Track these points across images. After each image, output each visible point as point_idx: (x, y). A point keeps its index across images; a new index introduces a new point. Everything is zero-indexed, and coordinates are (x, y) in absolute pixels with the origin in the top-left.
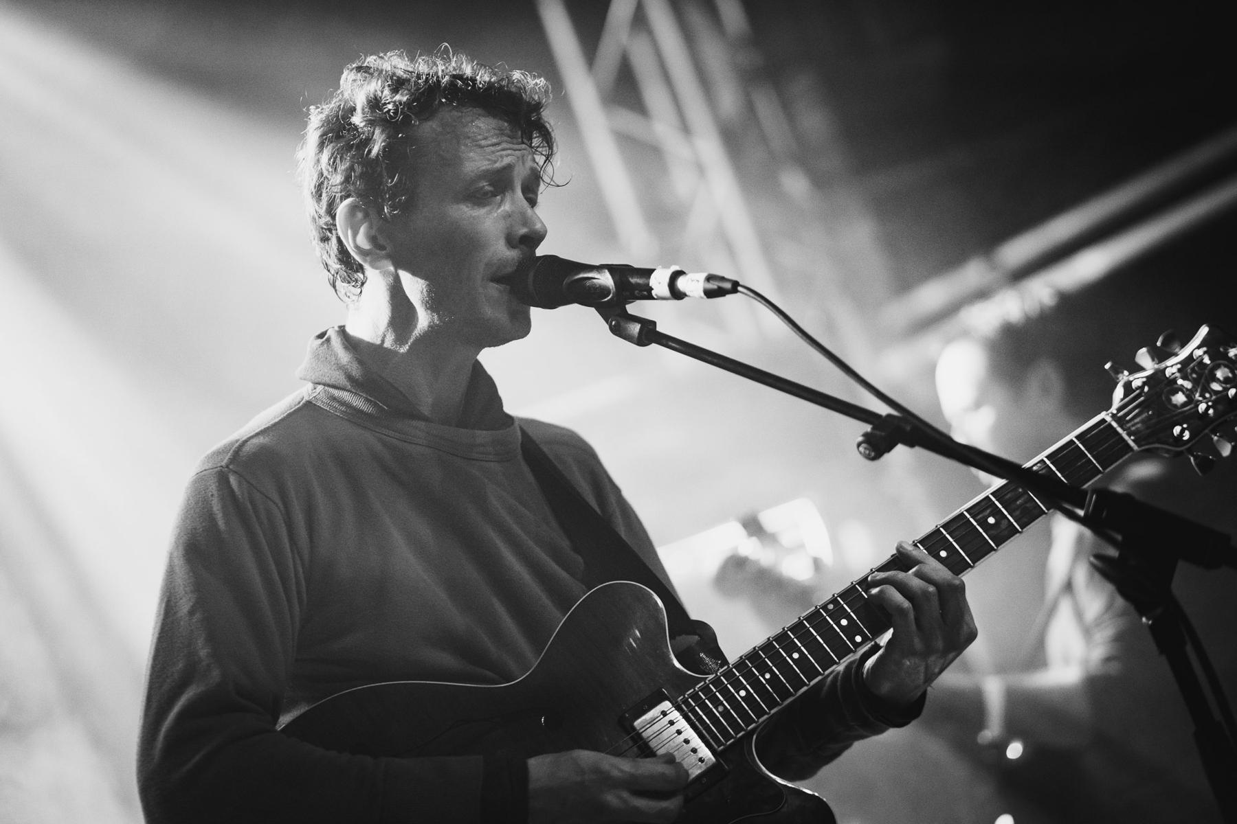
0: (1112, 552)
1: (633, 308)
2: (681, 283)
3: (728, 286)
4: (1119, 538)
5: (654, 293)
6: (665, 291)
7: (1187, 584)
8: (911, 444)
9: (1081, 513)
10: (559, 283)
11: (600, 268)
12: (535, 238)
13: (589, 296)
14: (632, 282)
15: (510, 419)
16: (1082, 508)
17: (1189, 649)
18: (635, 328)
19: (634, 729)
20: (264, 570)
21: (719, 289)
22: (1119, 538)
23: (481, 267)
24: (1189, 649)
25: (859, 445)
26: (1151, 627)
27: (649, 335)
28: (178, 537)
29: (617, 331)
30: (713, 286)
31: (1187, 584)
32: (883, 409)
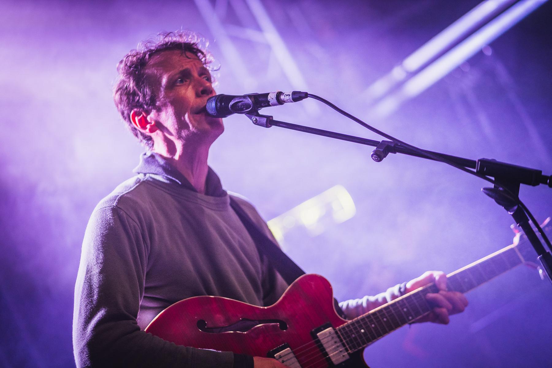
0: (492, 186)
1: (263, 111)
2: (282, 97)
3: (303, 95)
4: (493, 179)
5: (270, 103)
6: (275, 101)
7: (525, 193)
8: (395, 152)
9: (475, 170)
10: (227, 105)
11: (244, 97)
12: (208, 91)
13: (237, 109)
14: (260, 100)
15: (224, 193)
16: (161, 78)
17: (530, 222)
18: (264, 120)
19: (317, 337)
20: (133, 252)
21: (298, 96)
22: (493, 179)
23: (199, 100)
24: (530, 222)
25: (372, 156)
26: (512, 215)
27: (270, 122)
28: (99, 239)
29: (256, 123)
30: (295, 96)
31: (525, 193)
32: (380, 139)
